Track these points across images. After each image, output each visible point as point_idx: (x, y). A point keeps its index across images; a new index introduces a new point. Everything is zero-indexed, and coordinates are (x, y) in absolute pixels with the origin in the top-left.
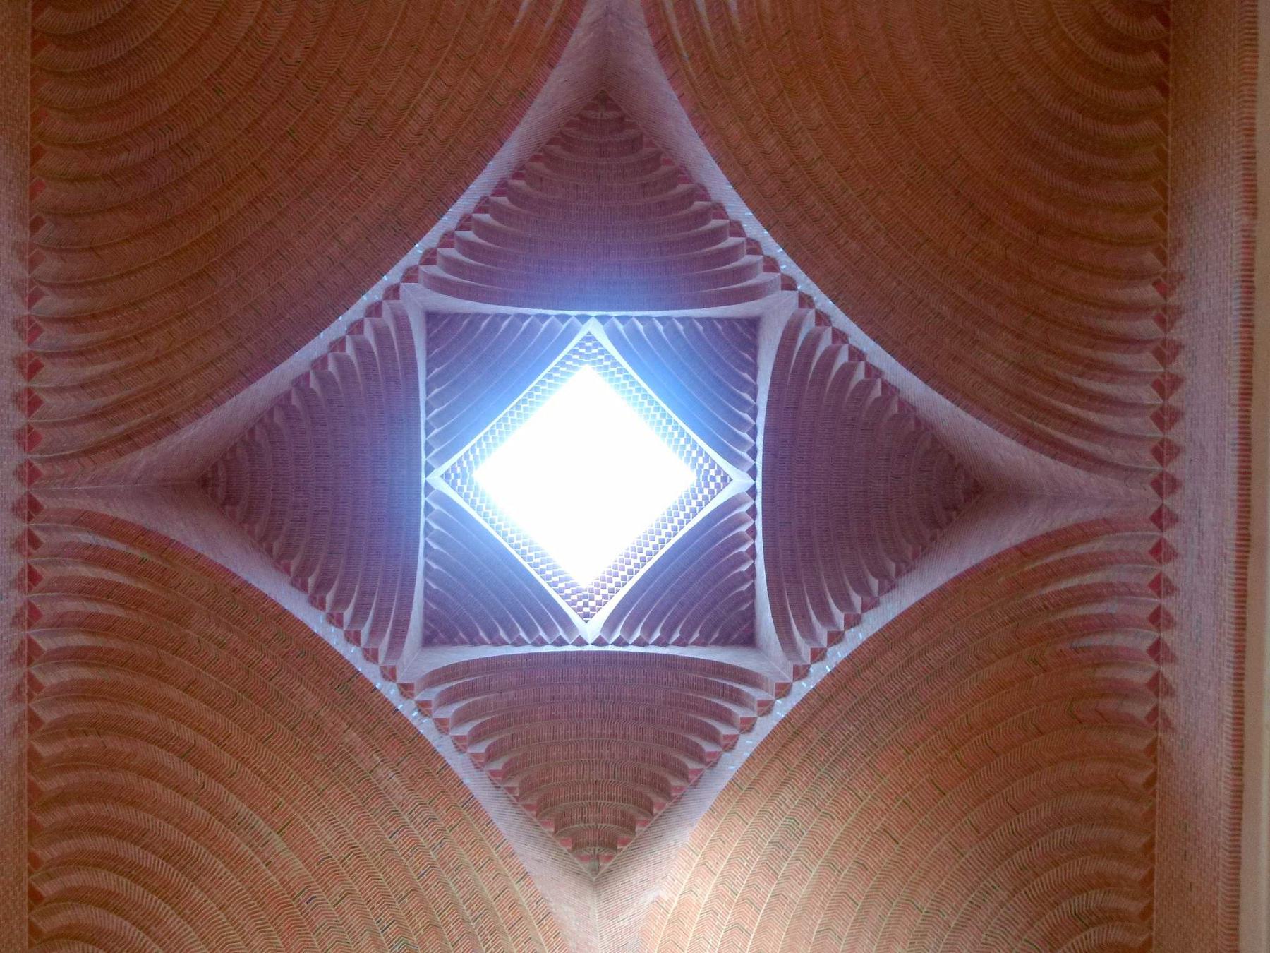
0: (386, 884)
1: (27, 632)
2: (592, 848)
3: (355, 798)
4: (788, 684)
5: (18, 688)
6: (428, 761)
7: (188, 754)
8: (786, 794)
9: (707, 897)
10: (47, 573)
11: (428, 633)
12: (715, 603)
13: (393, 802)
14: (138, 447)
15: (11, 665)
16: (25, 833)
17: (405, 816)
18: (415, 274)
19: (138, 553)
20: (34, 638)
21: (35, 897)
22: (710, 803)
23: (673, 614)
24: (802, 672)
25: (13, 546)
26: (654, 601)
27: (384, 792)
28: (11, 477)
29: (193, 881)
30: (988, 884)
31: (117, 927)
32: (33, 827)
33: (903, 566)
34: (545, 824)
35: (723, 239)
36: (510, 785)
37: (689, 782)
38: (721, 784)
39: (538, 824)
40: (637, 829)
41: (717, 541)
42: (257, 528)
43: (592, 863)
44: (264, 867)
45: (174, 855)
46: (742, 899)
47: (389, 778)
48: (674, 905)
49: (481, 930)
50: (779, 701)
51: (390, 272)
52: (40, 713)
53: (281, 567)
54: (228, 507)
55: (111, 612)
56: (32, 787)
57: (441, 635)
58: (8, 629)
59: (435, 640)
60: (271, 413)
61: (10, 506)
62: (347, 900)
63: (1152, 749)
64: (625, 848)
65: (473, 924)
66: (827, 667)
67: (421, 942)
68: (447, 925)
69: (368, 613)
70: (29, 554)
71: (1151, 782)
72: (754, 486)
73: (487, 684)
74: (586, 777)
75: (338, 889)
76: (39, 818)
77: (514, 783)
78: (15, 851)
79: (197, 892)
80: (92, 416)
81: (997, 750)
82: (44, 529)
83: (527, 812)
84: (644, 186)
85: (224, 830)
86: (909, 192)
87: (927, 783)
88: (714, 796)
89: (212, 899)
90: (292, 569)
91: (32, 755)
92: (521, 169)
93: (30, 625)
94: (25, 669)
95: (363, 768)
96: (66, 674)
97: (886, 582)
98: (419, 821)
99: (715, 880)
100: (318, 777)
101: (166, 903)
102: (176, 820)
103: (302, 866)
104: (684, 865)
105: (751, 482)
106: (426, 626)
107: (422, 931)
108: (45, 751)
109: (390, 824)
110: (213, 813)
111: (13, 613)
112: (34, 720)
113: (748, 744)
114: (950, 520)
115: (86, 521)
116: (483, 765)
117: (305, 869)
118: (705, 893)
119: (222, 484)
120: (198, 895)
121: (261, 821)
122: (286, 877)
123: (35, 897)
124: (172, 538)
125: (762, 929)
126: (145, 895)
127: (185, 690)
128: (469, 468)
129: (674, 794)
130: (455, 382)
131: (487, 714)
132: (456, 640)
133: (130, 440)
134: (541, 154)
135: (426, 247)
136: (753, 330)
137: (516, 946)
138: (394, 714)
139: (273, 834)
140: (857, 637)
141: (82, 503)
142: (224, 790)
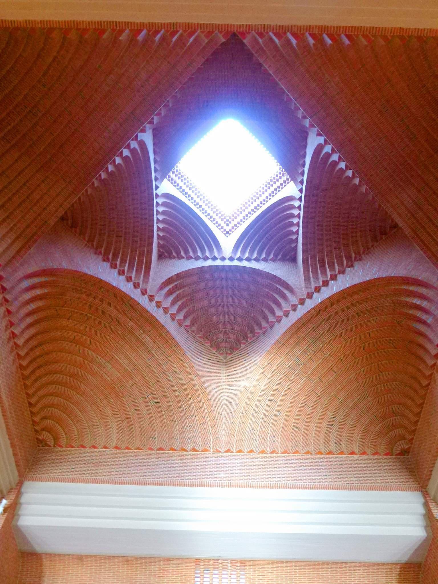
4: (304, 299)
5: (12, 349)
7: (73, 341)
11: (160, 253)
18: (152, 120)
21: (30, 404)
22: (268, 348)
30: (366, 394)
33: (358, 256)
34: (206, 343)
35: (266, 254)
37: (262, 331)
43: (225, 355)
45: (73, 376)
55: (38, 305)
56: (22, 374)
57: (166, 254)
59: (163, 256)
63: (431, 375)
66: (319, 299)
69: (134, 269)
71: (429, 384)
72: (301, 197)
73: (184, 283)
74: (223, 320)
75: (131, 382)
77: (194, 329)
81: (378, 349)
86: (379, 115)
87: (350, 354)
90: (102, 252)
91: (21, 365)
97: (350, 263)
99: (267, 379)
105: (301, 195)
106: (159, 251)
108: (24, 363)
110: (84, 358)
111: (5, 327)
113: (287, 323)
114: (381, 238)
123: (30, 404)
125: (282, 402)
129: (256, 335)
134: (202, 67)
141: (21, 273)
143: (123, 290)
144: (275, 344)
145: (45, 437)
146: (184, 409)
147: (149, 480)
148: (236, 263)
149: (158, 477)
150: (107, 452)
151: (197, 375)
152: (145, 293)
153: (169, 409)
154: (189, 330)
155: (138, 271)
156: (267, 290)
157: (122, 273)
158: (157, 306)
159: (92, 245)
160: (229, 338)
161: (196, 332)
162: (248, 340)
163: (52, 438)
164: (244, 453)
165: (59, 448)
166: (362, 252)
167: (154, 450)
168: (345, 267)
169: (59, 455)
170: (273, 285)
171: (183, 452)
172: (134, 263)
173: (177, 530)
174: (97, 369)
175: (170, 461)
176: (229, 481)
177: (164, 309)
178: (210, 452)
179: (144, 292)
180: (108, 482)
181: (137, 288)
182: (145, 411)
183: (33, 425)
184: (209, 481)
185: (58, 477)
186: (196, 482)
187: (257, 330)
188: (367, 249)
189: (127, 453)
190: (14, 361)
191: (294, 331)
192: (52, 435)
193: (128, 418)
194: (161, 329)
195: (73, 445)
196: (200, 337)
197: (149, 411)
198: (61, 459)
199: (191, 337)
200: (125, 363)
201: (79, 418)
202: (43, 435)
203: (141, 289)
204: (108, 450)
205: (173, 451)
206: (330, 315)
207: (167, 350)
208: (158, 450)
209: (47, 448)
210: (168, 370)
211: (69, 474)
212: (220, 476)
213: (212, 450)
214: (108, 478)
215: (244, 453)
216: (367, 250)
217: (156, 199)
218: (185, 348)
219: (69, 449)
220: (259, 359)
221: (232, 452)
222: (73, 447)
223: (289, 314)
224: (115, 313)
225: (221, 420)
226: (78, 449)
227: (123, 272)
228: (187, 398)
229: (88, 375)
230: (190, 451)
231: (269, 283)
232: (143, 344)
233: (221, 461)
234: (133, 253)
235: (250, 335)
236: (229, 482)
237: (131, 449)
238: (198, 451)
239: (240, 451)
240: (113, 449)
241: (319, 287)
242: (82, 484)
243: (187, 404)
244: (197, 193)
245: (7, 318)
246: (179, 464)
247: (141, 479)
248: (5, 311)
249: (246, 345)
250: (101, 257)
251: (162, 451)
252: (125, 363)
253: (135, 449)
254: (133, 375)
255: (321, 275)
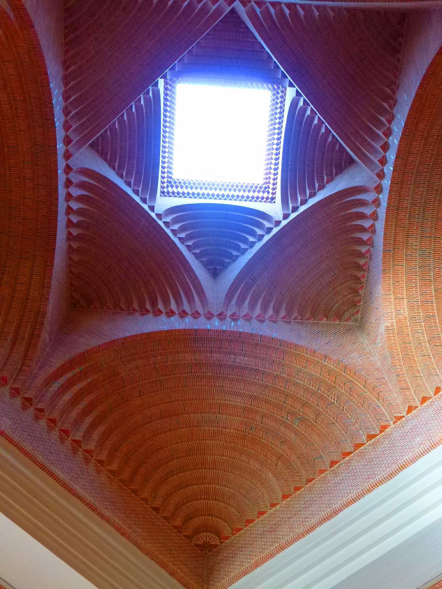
0: (274, 400)
1: (69, 439)
2: (348, 312)
3: (236, 377)
5: (86, 458)
6: (253, 339)
8: (412, 241)
9: (406, 312)
10: (55, 415)
11: (212, 271)
12: (323, 153)
13: (252, 367)
14: (39, 336)
15: (75, 455)
16: (133, 495)
17: (261, 369)
18: (69, 138)
19: (77, 370)
20: (73, 438)
21: (156, 509)
22: (381, 268)
23: (308, 173)
24: (382, 174)
25: (36, 420)
26: (295, 174)
27: (245, 366)
28: (11, 401)
29: (204, 455)
31: (192, 492)
32: (135, 491)
34: (321, 320)
36: (294, 317)
38: (380, 255)
39: (318, 322)
40: (361, 292)
41: (302, 124)
42: (109, 305)
44: (224, 430)
46: (422, 302)
47: (242, 360)
48: (395, 324)
49: (323, 392)
50: (381, 196)
51: (59, 167)
52: (100, 458)
53: (132, 312)
54: (91, 307)
58: (63, 446)
60: (71, 259)
61: (21, 409)
62: (264, 418)
64: (361, 303)
65: (319, 392)
66: (391, 168)
67: (304, 413)
68: (309, 399)
70: (44, 416)
74: (324, 283)
75: (258, 418)
76: (133, 487)
77: (295, 315)
78: (136, 504)
79: (209, 457)
80: (14, 344)
82: (39, 402)
83: (309, 321)
84: (124, 9)
85: (199, 429)
88: (381, 263)
89: (216, 455)
92: (65, 64)
93: (68, 436)
94: (81, 450)
95: (230, 364)
96: (96, 435)
97: (391, 101)
98: (268, 366)
99: (405, 301)
100: (216, 382)
101: (202, 469)
102: (179, 441)
103: (238, 418)
104: (388, 303)
107: (301, 409)
108: (114, 467)
109: (258, 377)
110: (190, 427)
111: (59, 440)
112: (100, 462)
114: (400, 44)
115: (48, 382)
116: (276, 318)
117: (240, 418)
118: (405, 312)
119: (80, 300)
120: (210, 458)
121: (209, 415)
122: (236, 427)
123: (156, 509)
124: (83, 351)
126: (192, 473)
127: (140, 396)
128: (171, 119)
130: (129, 158)
131: (263, 291)
132: (225, 265)
133: (34, 336)
134: (67, 47)
135: (62, 141)
136: (236, 16)
137: (342, 388)
138: (224, 333)
139: (217, 415)
140: (394, 141)
141: (43, 376)
142: (186, 416)
143: (181, 328)
144: (384, 256)
145: (205, 539)
146: (335, 403)
147: (338, 505)
148: (293, 216)
149: (346, 495)
150: (277, 509)
151: (326, 357)
152: (211, 316)
153: (318, 415)
154: (289, 320)
155: (190, 300)
156: (342, 214)
157: (171, 314)
158: (233, 320)
159: (122, 309)
160: (344, 296)
161: (298, 316)
162: (362, 280)
163: (214, 536)
164: (431, 397)
165: (228, 541)
166: (394, 80)
167: (327, 470)
168: (391, 111)
169: (231, 548)
170: (344, 203)
171: (361, 448)
172: (180, 296)
173: (406, 540)
174: (212, 428)
175: (351, 468)
176: (431, 440)
177: (245, 318)
178: (391, 427)
179: (209, 316)
180: (295, 540)
181: (198, 317)
182: (293, 436)
183: (180, 532)
184: (407, 457)
185: (240, 571)
186: (391, 469)
187: (362, 262)
188: (396, 71)
189: (300, 494)
190: (98, 472)
191: (394, 226)
192: (211, 532)
193: (279, 457)
194: (253, 339)
195: (239, 527)
196: (308, 319)
197: (297, 433)
198: (234, 550)
199: (296, 325)
200: (238, 401)
201: (228, 493)
202: (202, 538)
203: (204, 315)
204: (279, 506)
205: (348, 456)
206: (415, 173)
207: (275, 355)
208: (331, 467)
209: (215, 550)
210: (291, 376)
211: (249, 561)
212: (416, 442)
213: (392, 423)
214: (292, 535)
215: (431, 397)
216: (398, 71)
217: (161, 220)
218: (293, 340)
219: (237, 535)
220: (380, 287)
221: (416, 407)
222: (240, 530)
223: (377, 215)
224: (189, 357)
225: (386, 384)
226: (246, 528)
227: (173, 312)
228: (330, 388)
229: (207, 441)
230: (367, 442)
231: (338, 205)
232: (244, 368)
233: (409, 426)
234: (173, 288)
235: (360, 274)
236: (431, 441)
237: (303, 487)
238: (377, 435)
239: (424, 400)
240: (283, 501)
241: (383, 157)
242: (269, 561)
243: (334, 396)
244: (212, 186)
245: (57, 429)
246: (362, 464)
247: (329, 510)
248: (47, 423)
249: (364, 288)
250: (137, 314)
251: (337, 465)
252: (238, 401)
253: (306, 484)
254: (257, 409)
255: (376, 143)
